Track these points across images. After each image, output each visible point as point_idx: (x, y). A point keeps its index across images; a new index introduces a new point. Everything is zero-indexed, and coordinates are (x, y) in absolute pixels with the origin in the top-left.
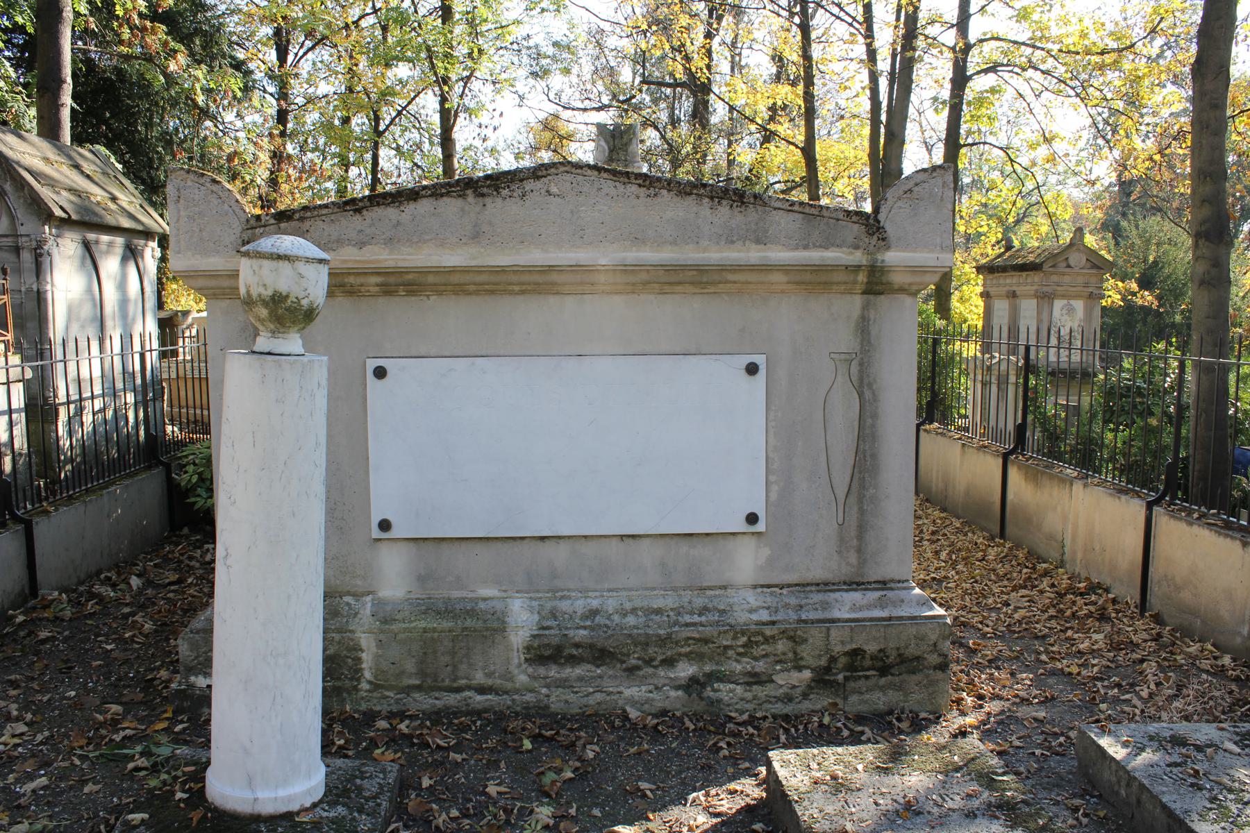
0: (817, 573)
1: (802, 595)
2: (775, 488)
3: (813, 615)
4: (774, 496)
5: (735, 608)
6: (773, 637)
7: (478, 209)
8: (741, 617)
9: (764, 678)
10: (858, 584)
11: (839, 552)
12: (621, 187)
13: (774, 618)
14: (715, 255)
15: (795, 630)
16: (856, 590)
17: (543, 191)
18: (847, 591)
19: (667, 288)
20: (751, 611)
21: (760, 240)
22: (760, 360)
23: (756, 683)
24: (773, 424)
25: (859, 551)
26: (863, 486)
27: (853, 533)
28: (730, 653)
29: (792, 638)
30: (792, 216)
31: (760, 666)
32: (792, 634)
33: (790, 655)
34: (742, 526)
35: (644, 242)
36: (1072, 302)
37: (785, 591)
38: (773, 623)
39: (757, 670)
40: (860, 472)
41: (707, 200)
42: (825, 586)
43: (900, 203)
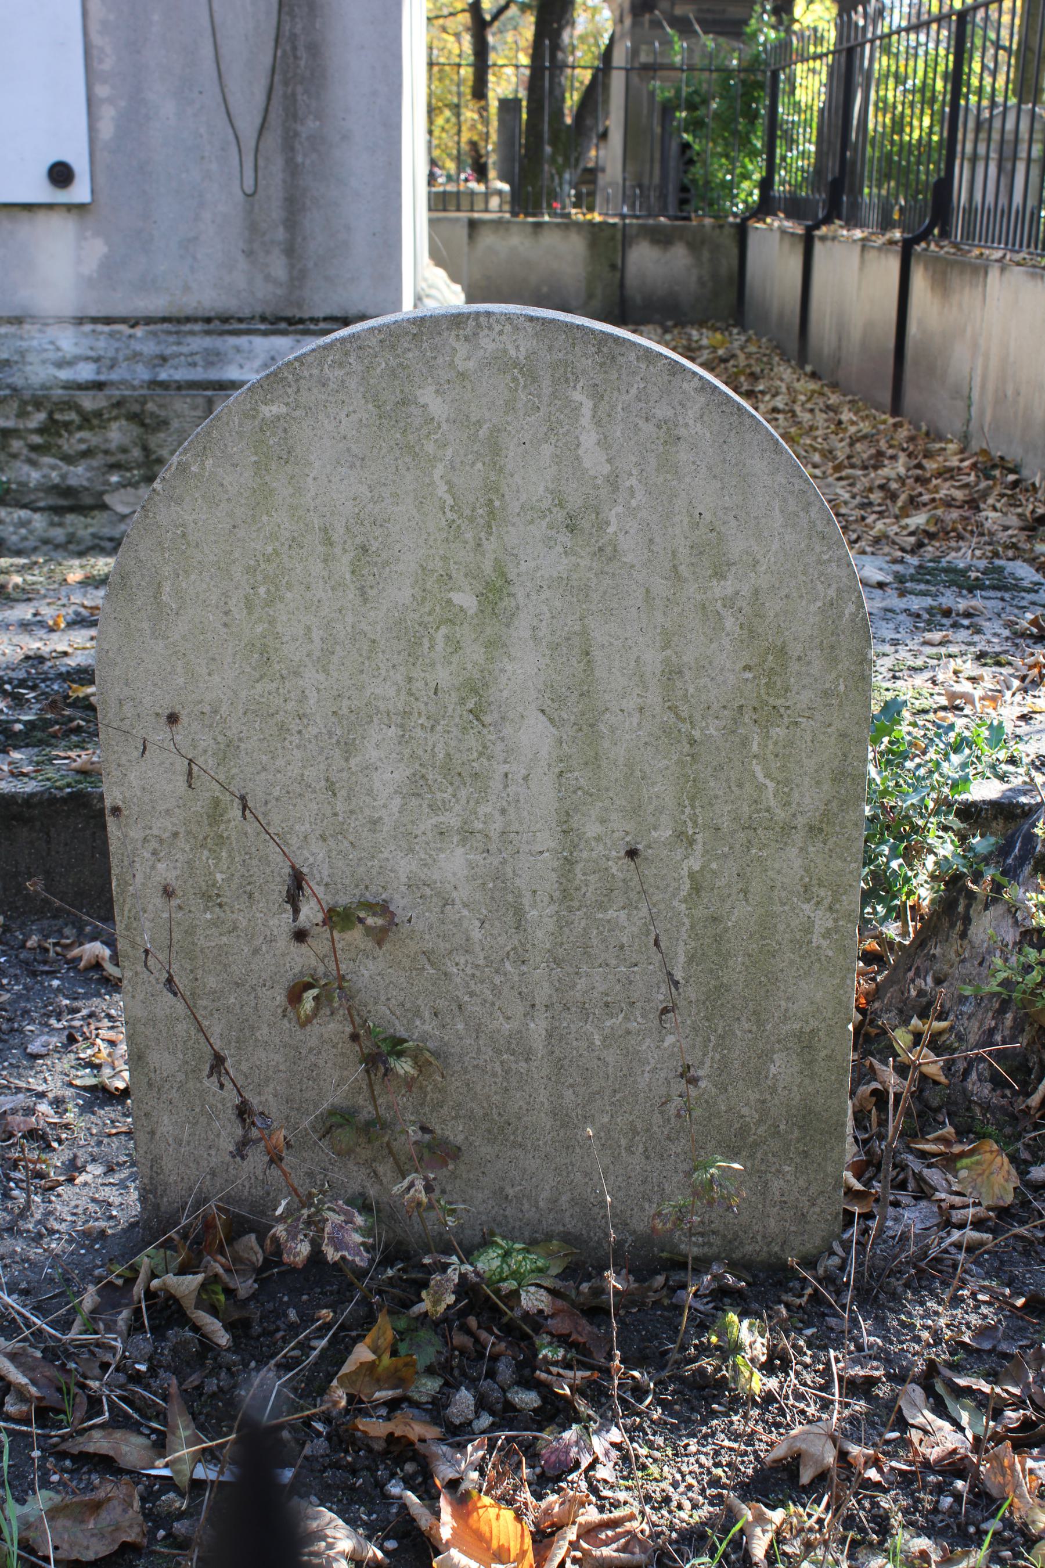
0: (205, 297)
1: (172, 339)
2: (108, 115)
3: (181, 374)
4: (107, 129)
5: (30, 358)
6: (98, 414)
8: (38, 373)
9: (88, 500)
10: (291, 321)
11: (249, 254)
13: (102, 378)
15: (143, 401)
16: (283, 333)
18: (265, 333)
20: (60, 364)
23: (72, 509)
25: (290, 251)
26: (292, 114)
27: (277, 213)
28: (16, 445)
29: (136, 418)
31: (79, 475)
32: (136, 408)
33: (136, 453)
34: (41, 192)
37: (139, 332)
38: (99, 386)
39: (72, 482)
40: (286, 83)
42: (222, 323)
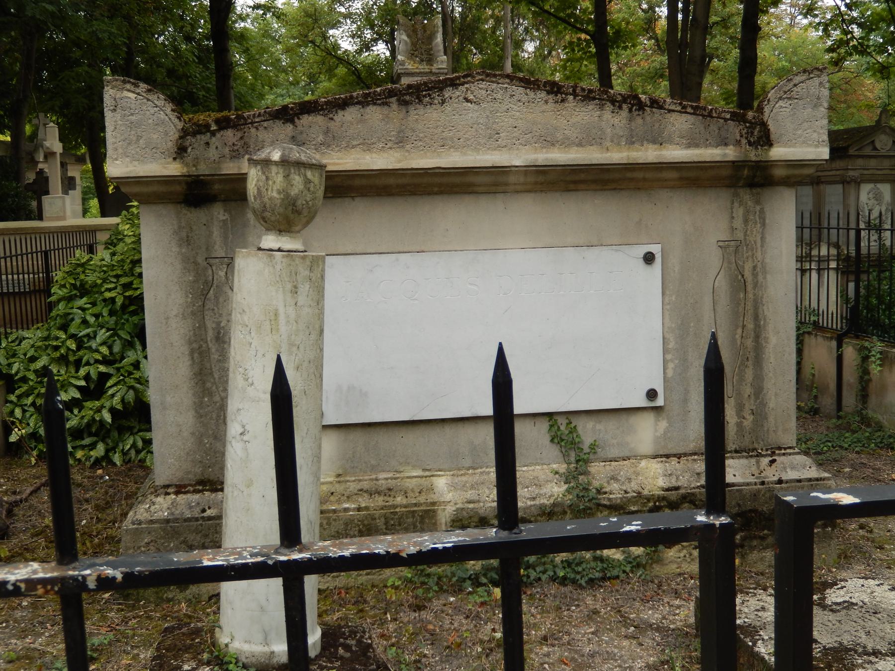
2: (671, 365)
4: (670, 373)
7: (401, 116)
12: (532, 94)
14: (617, 156)
17: (461, 98)
19: (572, 186)
21: (658, 140)
22: (656, 249)
24: (668, 307)
30: (685, 117)
35: (553, 145)
36: (879, 185)
41: (608, 104)
43: (781, 103)
